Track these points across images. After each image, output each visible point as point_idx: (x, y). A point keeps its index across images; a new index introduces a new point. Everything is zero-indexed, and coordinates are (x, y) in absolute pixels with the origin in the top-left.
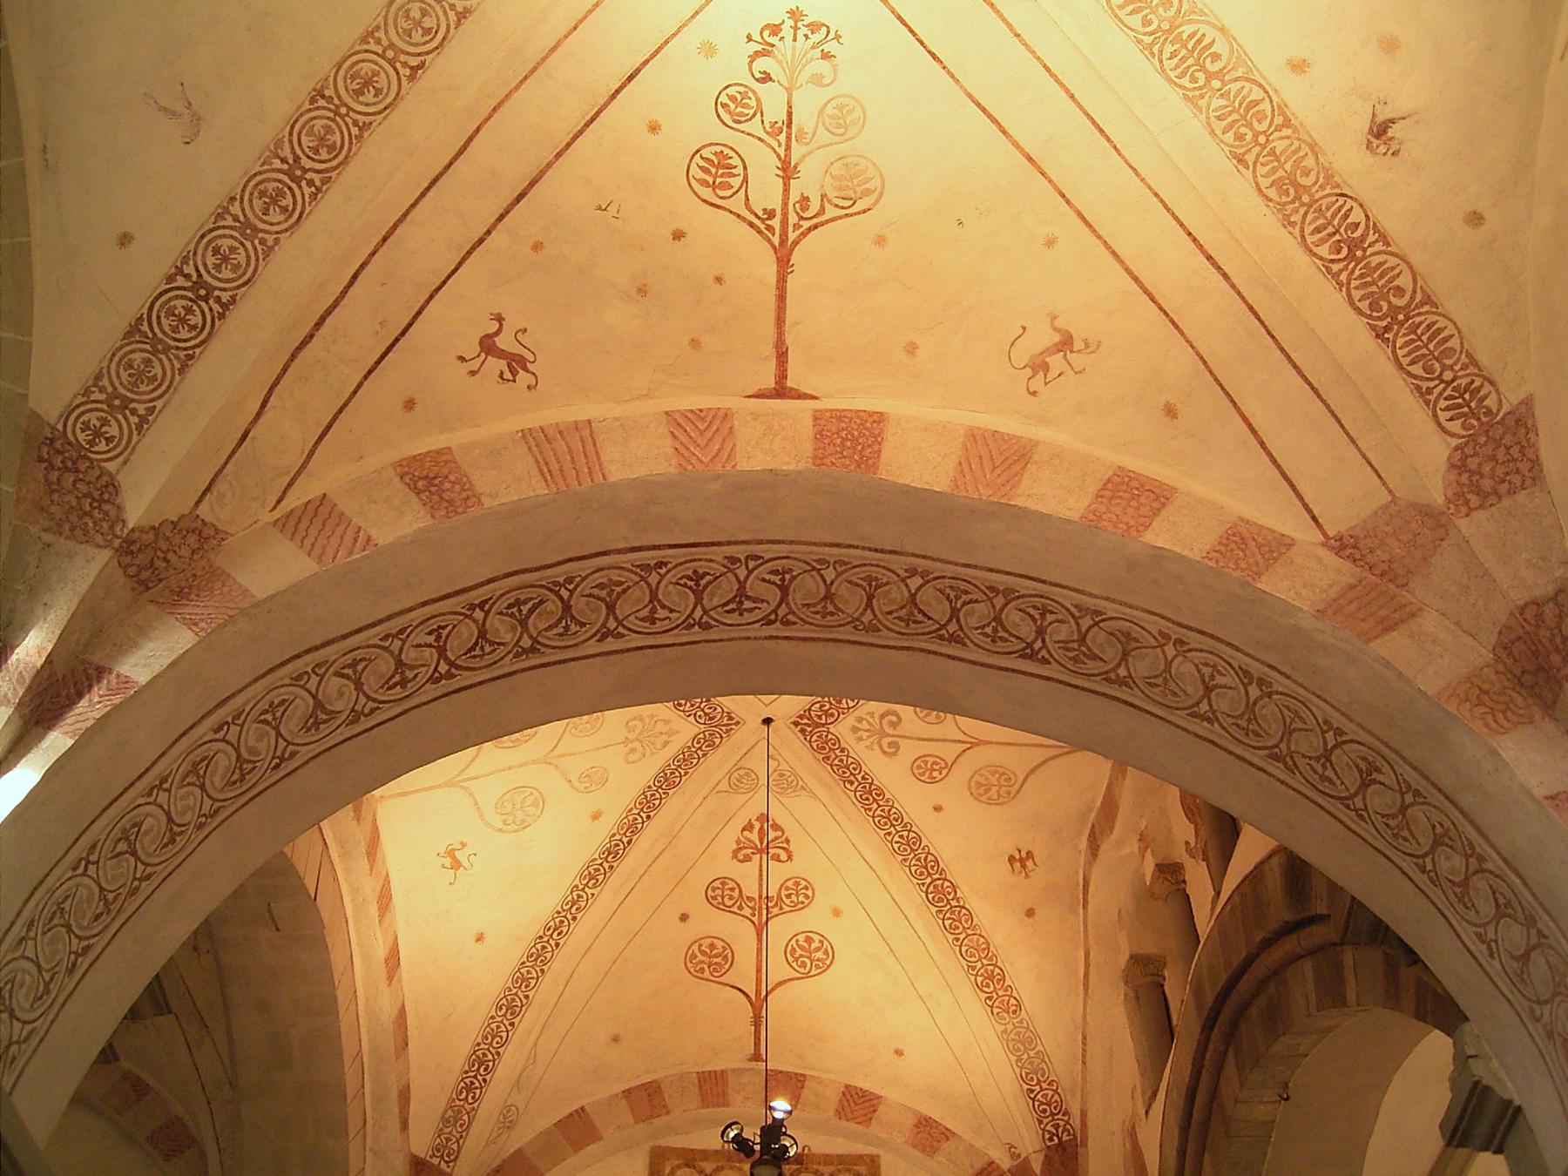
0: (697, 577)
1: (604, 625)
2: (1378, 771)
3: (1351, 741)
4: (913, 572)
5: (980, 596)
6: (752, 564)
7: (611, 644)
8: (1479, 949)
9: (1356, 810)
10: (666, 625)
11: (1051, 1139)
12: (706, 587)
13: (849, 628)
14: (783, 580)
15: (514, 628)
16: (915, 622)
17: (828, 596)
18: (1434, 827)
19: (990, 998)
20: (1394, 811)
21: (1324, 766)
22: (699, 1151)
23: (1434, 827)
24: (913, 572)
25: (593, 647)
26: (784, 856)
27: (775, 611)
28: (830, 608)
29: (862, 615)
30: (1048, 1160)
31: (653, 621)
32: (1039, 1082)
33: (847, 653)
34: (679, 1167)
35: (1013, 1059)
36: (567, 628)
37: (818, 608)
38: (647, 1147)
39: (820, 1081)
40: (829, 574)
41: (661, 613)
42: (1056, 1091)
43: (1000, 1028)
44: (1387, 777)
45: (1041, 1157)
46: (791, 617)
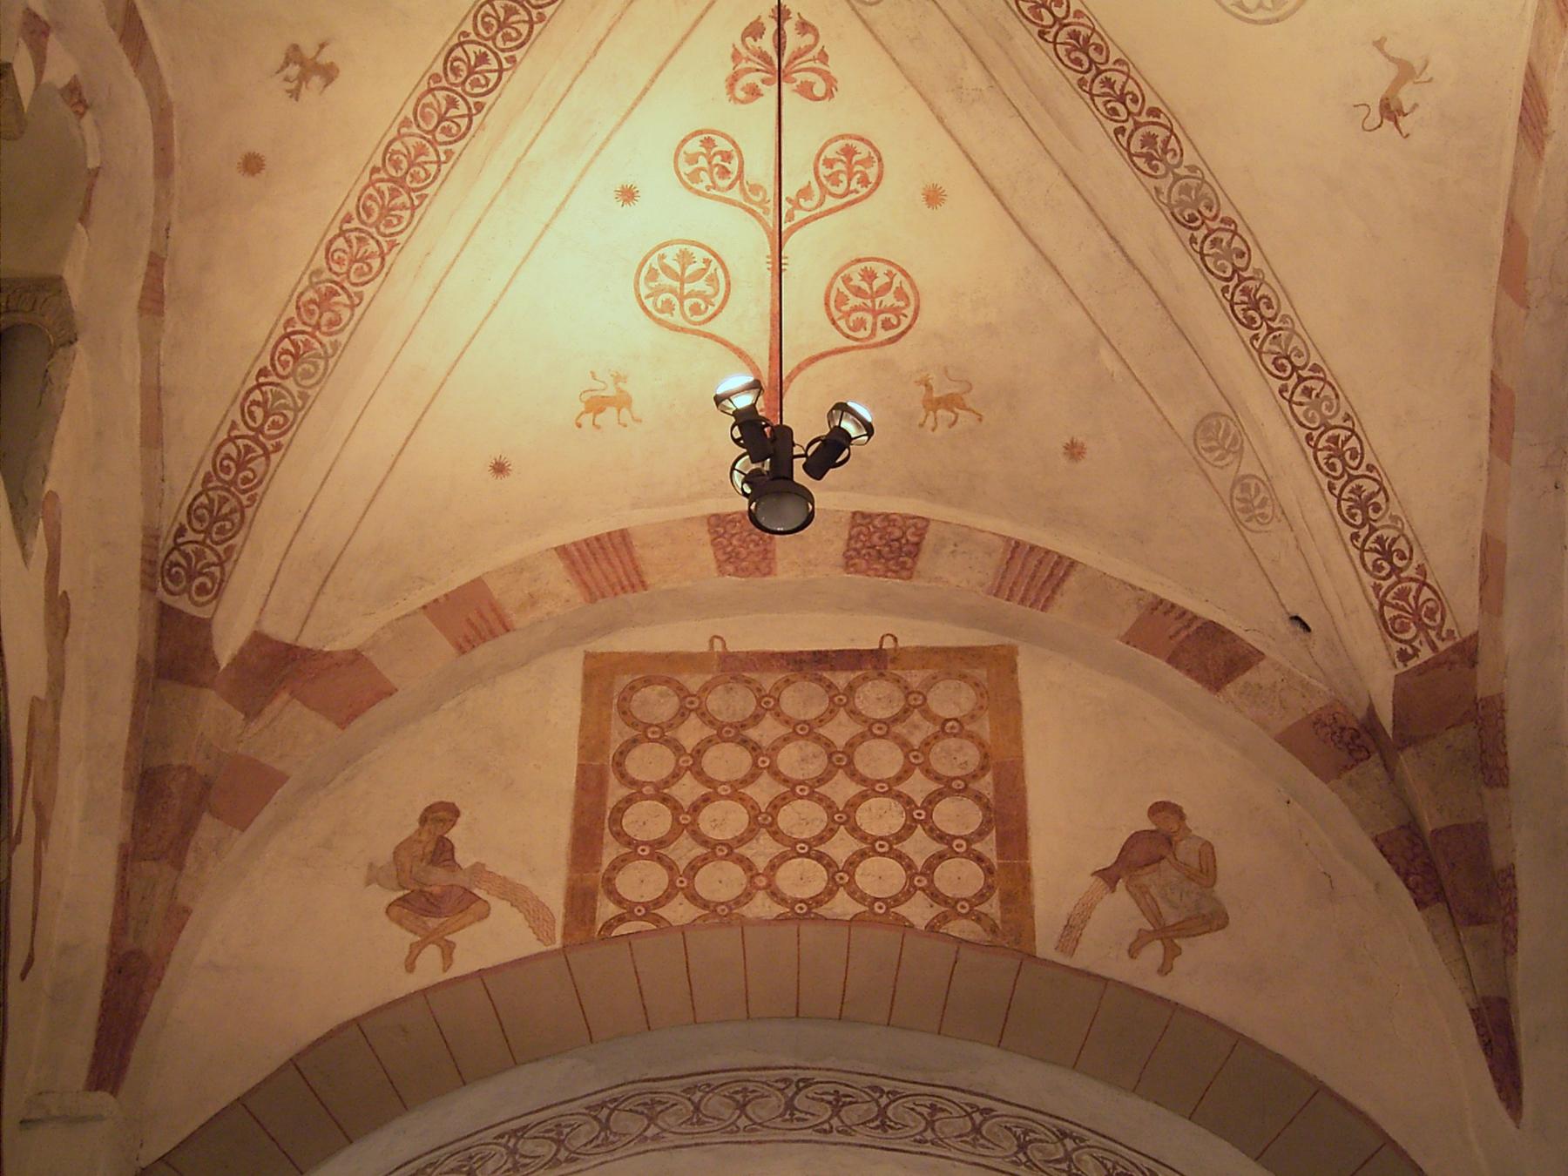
0: (883, 1127)
1: (985, 1120)
4: (656, 1138)
5: (582, 1150)
6: (826, 1126)
7: (983, 1103)
10: (919, 1100)
12: (876, 1118)
13: (716, 1083)
14: (792, 1114)
15: (1079, 1161)
16: (645, 1104)
17: (742, 1107)
24: (656, 1138)
25: (1001, 1108)
26: (820, 89)
27: (800, 1090)
28: (739, 1097)
29: (702, 1098)
31: (932, 1107)
33: (716, 1063)
36: (1025, 1134)
37: (751, 1096)
40: (743, 1122)
41: (925, 1111)
46: (781, 1085)
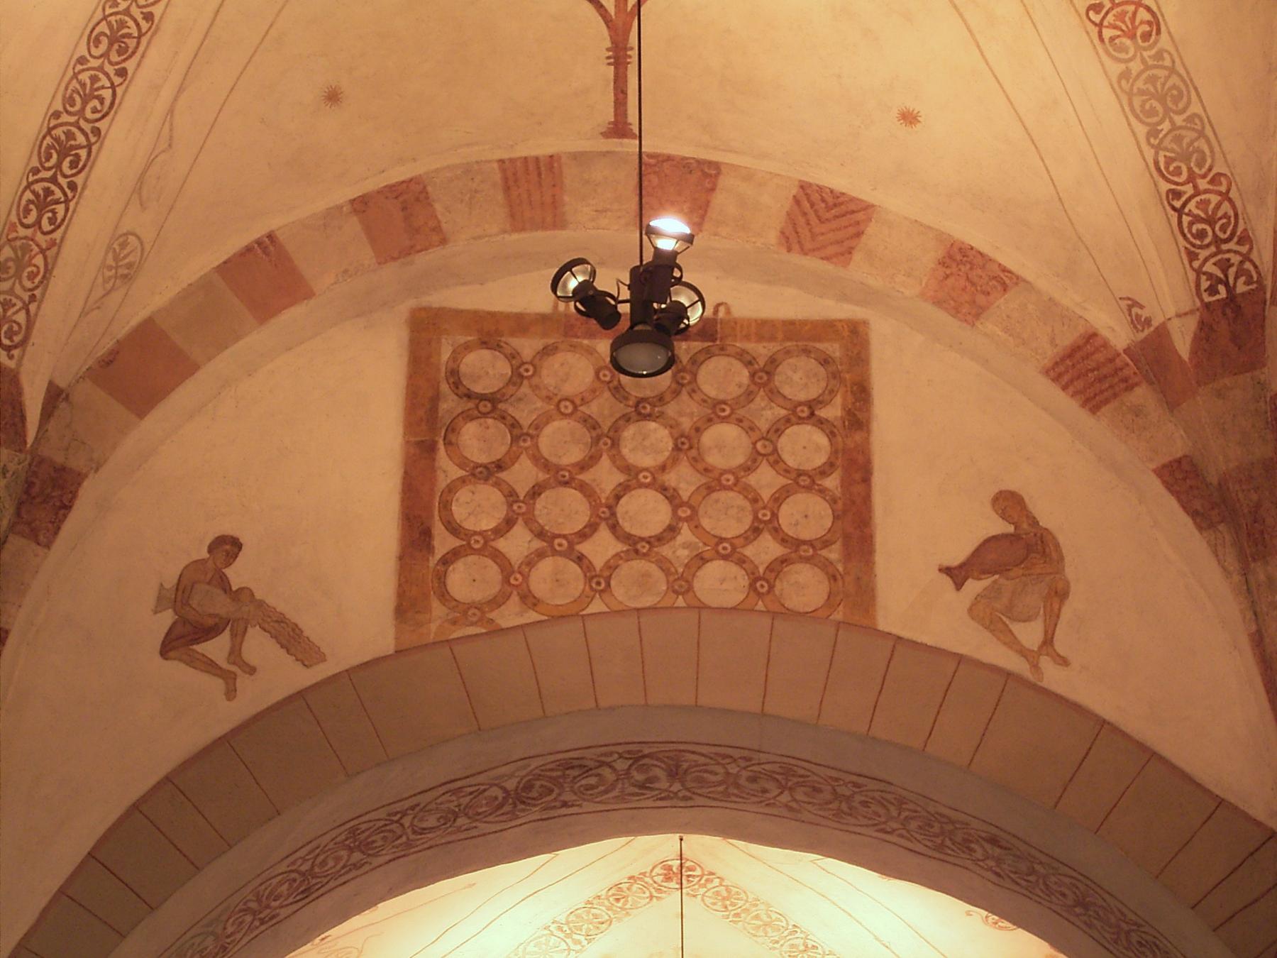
11: (1212, 290)
22: (508, 316)
30: (1205, 331)
32: (1192, 179)
34: (467, 348)
35: (1142, 130)
42: (1226, 196)
43: (1115, 69)
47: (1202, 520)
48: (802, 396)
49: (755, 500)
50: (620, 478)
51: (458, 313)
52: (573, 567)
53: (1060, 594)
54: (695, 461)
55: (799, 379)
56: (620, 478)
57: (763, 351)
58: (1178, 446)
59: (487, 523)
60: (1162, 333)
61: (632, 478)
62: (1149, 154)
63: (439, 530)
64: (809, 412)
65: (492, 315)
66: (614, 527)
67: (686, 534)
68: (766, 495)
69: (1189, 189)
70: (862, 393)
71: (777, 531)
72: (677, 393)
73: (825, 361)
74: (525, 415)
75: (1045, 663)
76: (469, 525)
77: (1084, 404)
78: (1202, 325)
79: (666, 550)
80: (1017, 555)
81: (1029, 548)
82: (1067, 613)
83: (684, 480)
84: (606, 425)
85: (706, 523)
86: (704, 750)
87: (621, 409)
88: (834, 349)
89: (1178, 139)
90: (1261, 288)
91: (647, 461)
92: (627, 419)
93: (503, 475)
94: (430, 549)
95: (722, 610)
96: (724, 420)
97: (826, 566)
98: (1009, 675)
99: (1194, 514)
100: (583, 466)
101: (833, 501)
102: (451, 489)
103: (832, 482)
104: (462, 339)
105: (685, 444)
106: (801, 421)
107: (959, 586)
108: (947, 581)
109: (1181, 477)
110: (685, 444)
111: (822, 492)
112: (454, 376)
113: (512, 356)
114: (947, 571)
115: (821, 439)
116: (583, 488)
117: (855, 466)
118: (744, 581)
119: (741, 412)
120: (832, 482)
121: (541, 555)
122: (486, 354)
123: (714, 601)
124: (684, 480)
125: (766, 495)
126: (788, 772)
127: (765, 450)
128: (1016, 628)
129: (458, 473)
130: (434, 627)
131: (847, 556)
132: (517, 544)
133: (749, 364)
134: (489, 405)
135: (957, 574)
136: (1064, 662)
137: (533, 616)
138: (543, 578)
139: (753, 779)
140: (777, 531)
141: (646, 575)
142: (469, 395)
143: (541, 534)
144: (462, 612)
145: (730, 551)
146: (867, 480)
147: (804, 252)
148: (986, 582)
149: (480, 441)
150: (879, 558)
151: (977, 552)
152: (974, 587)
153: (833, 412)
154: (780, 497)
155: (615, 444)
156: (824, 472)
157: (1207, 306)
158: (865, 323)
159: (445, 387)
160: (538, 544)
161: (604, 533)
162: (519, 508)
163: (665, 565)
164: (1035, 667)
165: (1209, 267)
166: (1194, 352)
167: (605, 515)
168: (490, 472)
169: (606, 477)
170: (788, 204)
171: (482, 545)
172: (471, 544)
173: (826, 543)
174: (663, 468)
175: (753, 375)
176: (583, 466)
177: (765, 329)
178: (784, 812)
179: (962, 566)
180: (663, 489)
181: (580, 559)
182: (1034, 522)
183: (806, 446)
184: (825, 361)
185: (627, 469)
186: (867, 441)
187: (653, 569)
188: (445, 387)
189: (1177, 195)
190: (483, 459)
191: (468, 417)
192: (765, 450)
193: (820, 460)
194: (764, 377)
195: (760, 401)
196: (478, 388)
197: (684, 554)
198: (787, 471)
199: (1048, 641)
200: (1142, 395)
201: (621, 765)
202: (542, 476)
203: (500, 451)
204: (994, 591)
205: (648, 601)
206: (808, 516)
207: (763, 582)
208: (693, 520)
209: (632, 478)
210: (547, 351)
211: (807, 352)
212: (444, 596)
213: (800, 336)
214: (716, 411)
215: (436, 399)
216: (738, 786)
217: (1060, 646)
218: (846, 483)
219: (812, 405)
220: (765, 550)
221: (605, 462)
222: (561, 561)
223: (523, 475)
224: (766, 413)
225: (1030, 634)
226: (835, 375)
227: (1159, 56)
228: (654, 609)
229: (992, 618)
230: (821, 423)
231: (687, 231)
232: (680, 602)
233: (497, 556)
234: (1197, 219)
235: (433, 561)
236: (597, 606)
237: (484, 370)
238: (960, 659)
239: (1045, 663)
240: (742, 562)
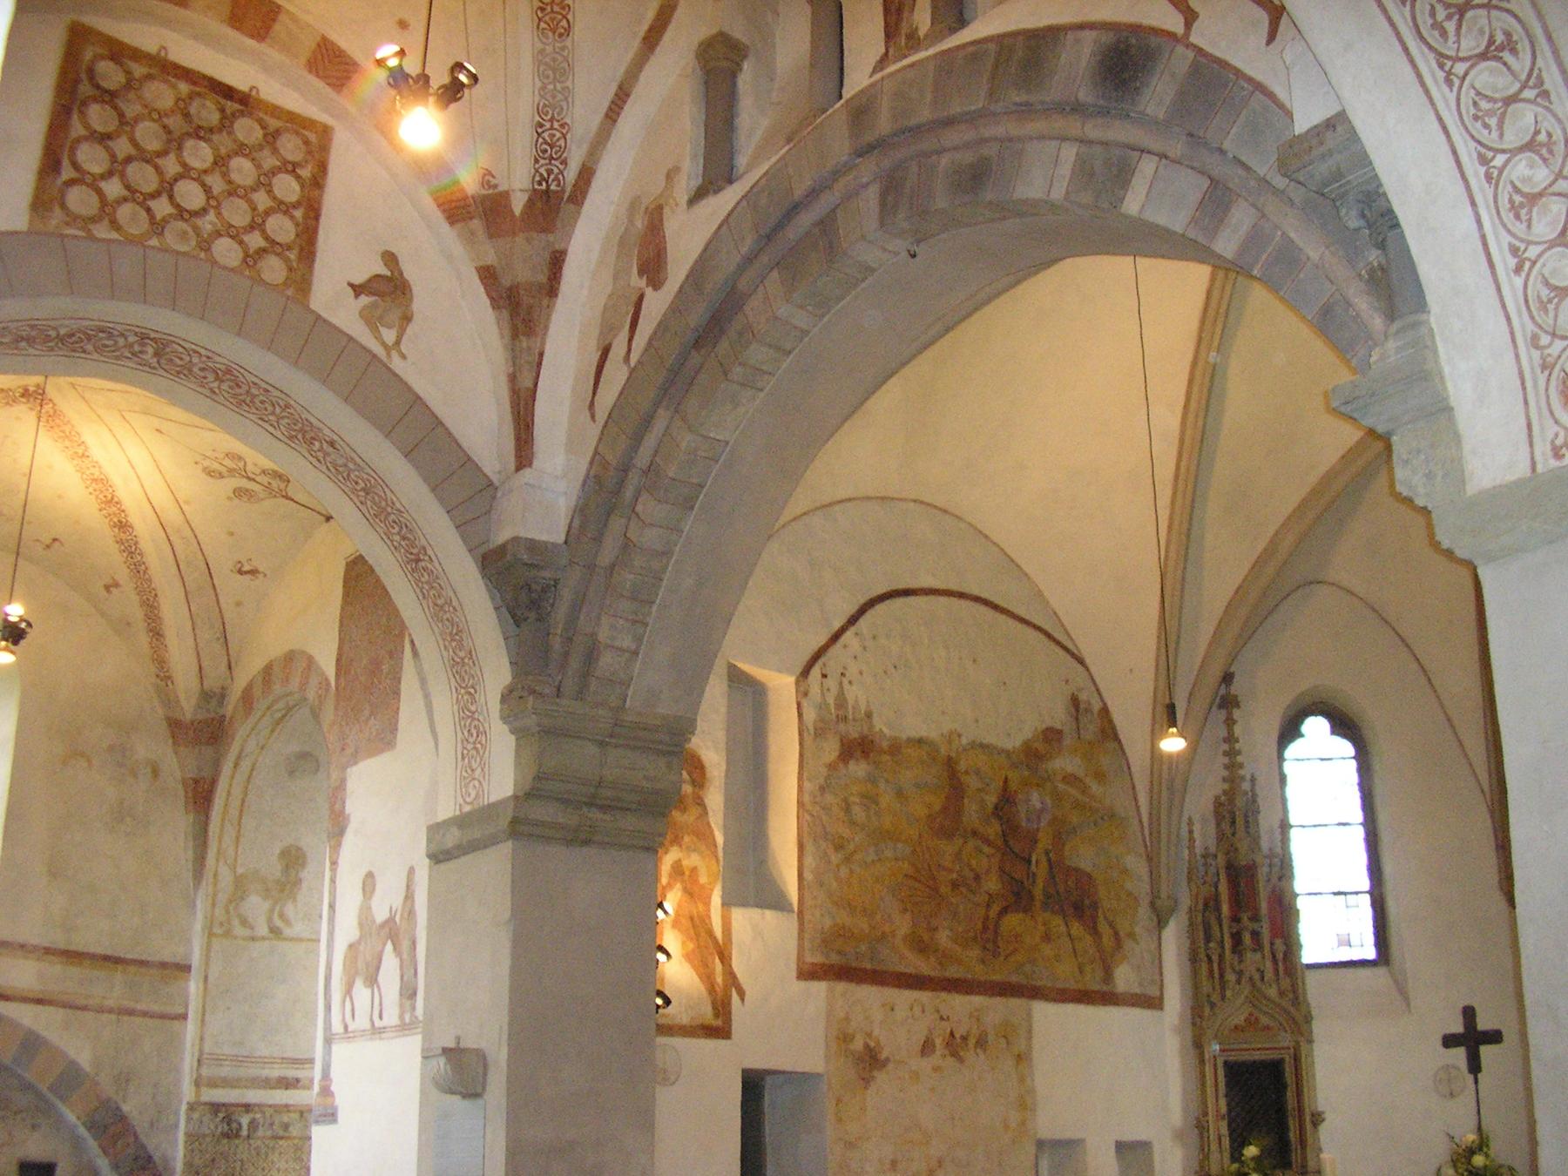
2: (1514, 51)
3: (1508, 11)
8: (1505, 262)
9: (1449, 73)
11: (540, 183)
18: (1537, 132)
19: (542, 9)
20: (1497, 96)
21: (1449, 17)
22: (129, 48)
23: (1537, 132)
30: (530, 203)
32: (551, 120)
34: (102, 58)
35: (539, 84)
38: (69, 18)
39: (295, 19)
42: (564, 136)
43: (539, 46)
44: (1521, 64)
45: (524, 198)
47: (495, 303)
48: (290, 158)
49: (254, 209)
50: (179, 169)
51: (99, 34)
52: (144, 214)
53: (407, 318)
54: (225, 175)
55: (290, 147)
56: (179, 169)
57: (274, 123)
58: (490, 258)
59: (97, 169)
60: (505, 195)
61: (186, 172)
62: (537, 99)
63: (66, 162)
64: (292, 168)
65: (121, 44)
66: (171, 197)
67: (211, 216)
68: (261, 208)
69: (548, 125)
70: (323, 168)
71: (263, 232)
72: (220, 131)
73: (307, 142)
74: (131, 110)
75: (394, 353)
76: (86, 166)
77: (448, 218)
78: (530, 199)
79: (199, 222)
80: (388, 289)
81: (396, 287)
82: (409, 331)
83: (217, 183)
84: (176, 134)
85: (225, 213)
86: (187, 345)
87: (187, 128)
88: (312, 137)
89: (554, 97)
90: (563, 191)
91: (196, 164)
92: (188, 134)
93: (110, 143)
94: (59, 173)
95: (225, 268)
96: (245, 156)
97: (287, 260)
98: (374, 356)
99: (492, 299)
100: (159, 154)
101: (297, 225)
102: (78, 141)
103: (298, 214)
104: (100, 51)
105: (220, 163)
106: (287, 172)
107: (357, 296)
108: (350, 291)
109: (488, 275)
110: (220, 163)
111: (292, 217)
112: (91, 72)
113: (128, 72)
114: (351, 285)
115: (296, 186)
116: (157, 167)
117: (313, 210)
118: (241, 255)
119: (255, 154)
120: (298, 214)
121: (126, 200)
122: (111, 64)
123: (222, 261)
124: (217, 183)
125: (261, 208)
126: (228, 371)
127: (264, 182)
128: (383, 330)
129: (82, 132)
130: (54, 222)
131: (300, 259)
132: (113, 188)
133: (263, 128)
134: (109, 97)
135: (358, 290)
136: (404, 357)
137: (114, 235)
138: (124, 212)
139: (202, 369)
140: (263, 232)
141: (185, 233)
142: (98, 87)
143: (128, 187)
144: (73, 219)
145: (236, 235)
146: (317, 218)
147: (318, 76)
148: (373, 298)
149: (99, 117)
150: (318, 265)
151: (370, 280)
152: (365, 300)
153: (305, 173)
154: (267, 213)
155: (180, 148)
156: (295, 206)
157: (535, 190)
158: (332, 129)
159: (83, 76)
160: (126, 193)
161: (164, 199)
162: (117, 168)
163: (196, 229)
164: (389, 355)
165: (543, 171)
166: (522, 213)
167: (167, 188)
168: (104, 138)
169: (171, 166)
170: (314, 46)
171: (93, 182)
172: (82, 178)
173: (289, 248)
174: (205, 172)
175: (265, 135)
176: (159, 154)
177: (276, 111)
178: (207, 392)
179: (360, 286)
180: (203, 185)
181: (148, 210)
182: (401, 274)
183: (287, 187)
184: (307, 142)
185: (184, 165)
186: (321, 196)
187: (189, 230)
188: (83, 76)
189: (541, 126)
190: (100, 129)
191: (95, 100)
192: (264, 182)
193: (293, 198)
194: (271, 137)
195: (266, 152)
196: (105, 84)
197: (209, 227)
198: (275, 198)
199: (398, 342)
200: (476, 224)
201: (132, 339)
202: (133, 152)
203: (111, 128)
204: (374, 306)
205: (184, 248)
206: (282, 228)
207: (252, 259)
208: (218, 207)
209: (186, 172)
210: (149, 77)
211: (297, 133)
212: (63, 206)
213: (298, 123)
214: (241, 150)
215: (77, 81)
216: (190, 371)
217: (403, 348)
218: (306, 217)
219: (295, 165)
220: (255, 241)
221: (172, 156)
222: (137, 208)
223: (122, 147)
224: (270, 162)
225: (389, 336)
226: (309, 152)
227: (563, 49)
228: (184, 254)
229: (372, 320)
230: (298, 177)
231: (397, 48)
232: (202, 255)
233: (100, 192)
234: (546, 143)
235: (59, 182)
236: (154, 242)
237: (110, 74)
238: (351, 339)
239: (394, 353)
240: (241, 243)
